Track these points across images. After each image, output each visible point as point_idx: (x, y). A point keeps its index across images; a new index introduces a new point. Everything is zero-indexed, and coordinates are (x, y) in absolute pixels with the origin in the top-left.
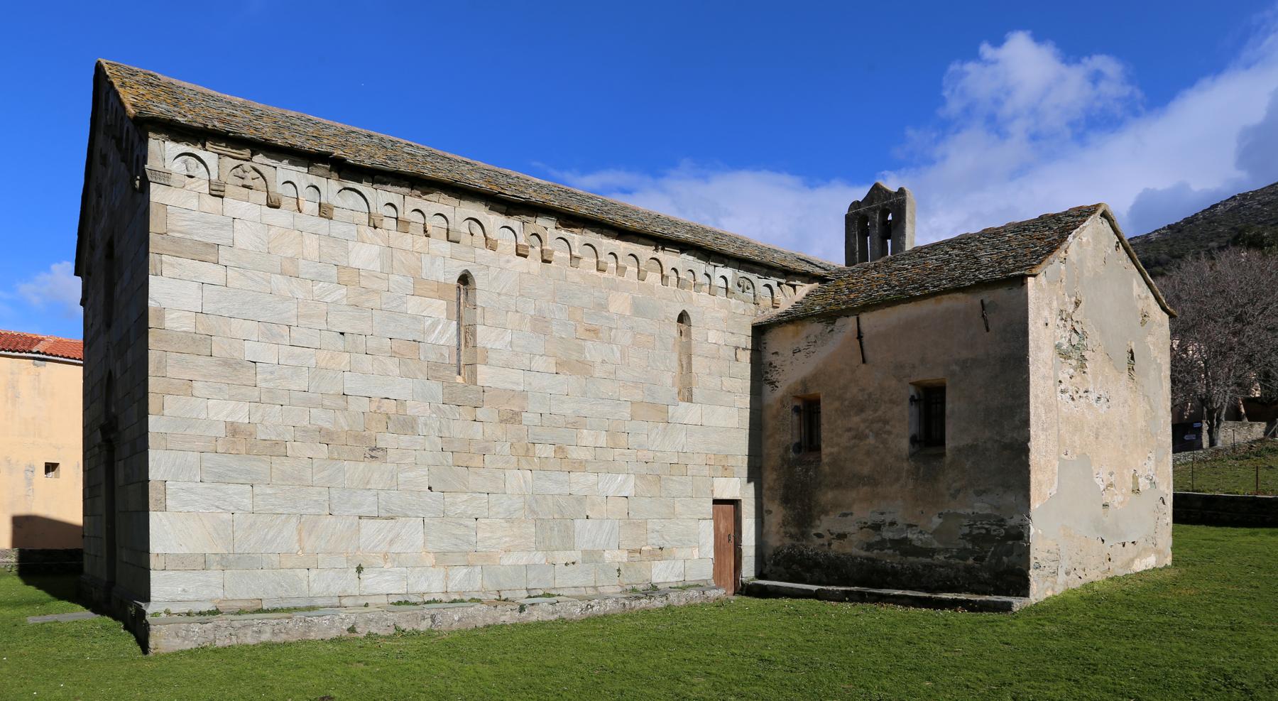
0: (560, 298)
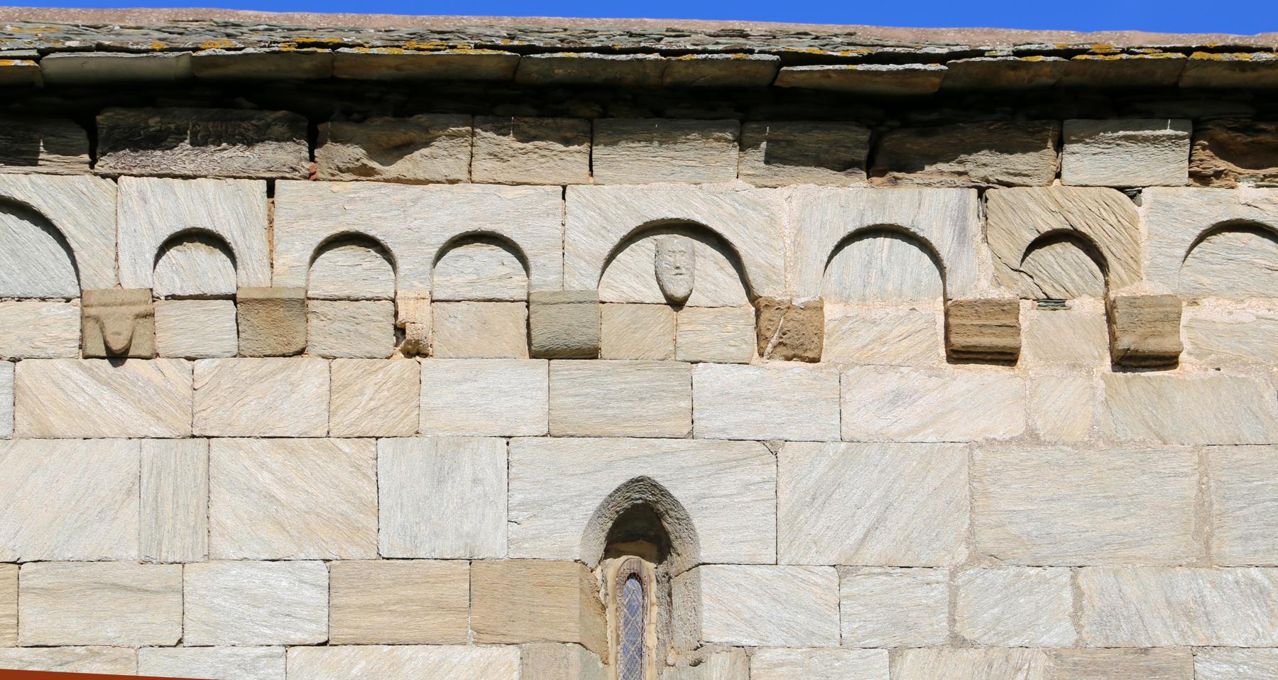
0: (1246, 538)
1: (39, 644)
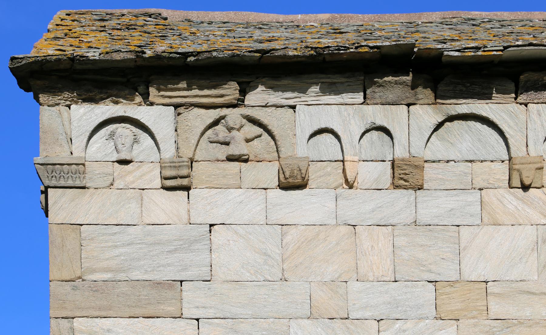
1: (497, 318)
